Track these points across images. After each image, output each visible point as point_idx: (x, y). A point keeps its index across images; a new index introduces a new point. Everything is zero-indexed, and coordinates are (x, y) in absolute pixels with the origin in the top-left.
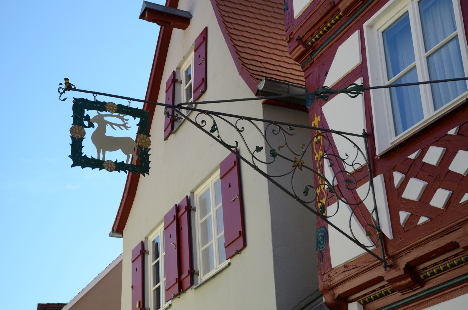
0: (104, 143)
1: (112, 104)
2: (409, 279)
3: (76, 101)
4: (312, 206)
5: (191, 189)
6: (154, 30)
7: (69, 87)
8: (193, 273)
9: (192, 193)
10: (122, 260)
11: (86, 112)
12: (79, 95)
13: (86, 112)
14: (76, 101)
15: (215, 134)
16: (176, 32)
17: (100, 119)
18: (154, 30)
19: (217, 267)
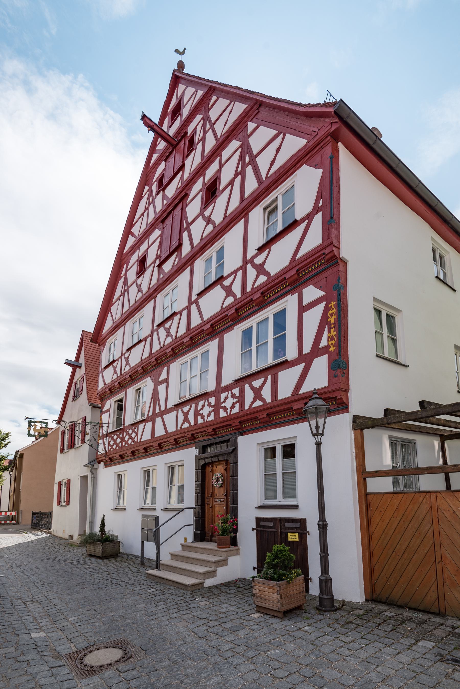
0: (35, 430)
2: (269, 377)
3: (29, 421)
6: (70, 369)
7: (27, 418)
8: (74, 444)
10: (223, 247)
11: (31, 424)
12: (29, 420)
13: (31, 424)
14: (29, 421)
16: (78, 369)
18: (70, 369)
19: (80, 445)
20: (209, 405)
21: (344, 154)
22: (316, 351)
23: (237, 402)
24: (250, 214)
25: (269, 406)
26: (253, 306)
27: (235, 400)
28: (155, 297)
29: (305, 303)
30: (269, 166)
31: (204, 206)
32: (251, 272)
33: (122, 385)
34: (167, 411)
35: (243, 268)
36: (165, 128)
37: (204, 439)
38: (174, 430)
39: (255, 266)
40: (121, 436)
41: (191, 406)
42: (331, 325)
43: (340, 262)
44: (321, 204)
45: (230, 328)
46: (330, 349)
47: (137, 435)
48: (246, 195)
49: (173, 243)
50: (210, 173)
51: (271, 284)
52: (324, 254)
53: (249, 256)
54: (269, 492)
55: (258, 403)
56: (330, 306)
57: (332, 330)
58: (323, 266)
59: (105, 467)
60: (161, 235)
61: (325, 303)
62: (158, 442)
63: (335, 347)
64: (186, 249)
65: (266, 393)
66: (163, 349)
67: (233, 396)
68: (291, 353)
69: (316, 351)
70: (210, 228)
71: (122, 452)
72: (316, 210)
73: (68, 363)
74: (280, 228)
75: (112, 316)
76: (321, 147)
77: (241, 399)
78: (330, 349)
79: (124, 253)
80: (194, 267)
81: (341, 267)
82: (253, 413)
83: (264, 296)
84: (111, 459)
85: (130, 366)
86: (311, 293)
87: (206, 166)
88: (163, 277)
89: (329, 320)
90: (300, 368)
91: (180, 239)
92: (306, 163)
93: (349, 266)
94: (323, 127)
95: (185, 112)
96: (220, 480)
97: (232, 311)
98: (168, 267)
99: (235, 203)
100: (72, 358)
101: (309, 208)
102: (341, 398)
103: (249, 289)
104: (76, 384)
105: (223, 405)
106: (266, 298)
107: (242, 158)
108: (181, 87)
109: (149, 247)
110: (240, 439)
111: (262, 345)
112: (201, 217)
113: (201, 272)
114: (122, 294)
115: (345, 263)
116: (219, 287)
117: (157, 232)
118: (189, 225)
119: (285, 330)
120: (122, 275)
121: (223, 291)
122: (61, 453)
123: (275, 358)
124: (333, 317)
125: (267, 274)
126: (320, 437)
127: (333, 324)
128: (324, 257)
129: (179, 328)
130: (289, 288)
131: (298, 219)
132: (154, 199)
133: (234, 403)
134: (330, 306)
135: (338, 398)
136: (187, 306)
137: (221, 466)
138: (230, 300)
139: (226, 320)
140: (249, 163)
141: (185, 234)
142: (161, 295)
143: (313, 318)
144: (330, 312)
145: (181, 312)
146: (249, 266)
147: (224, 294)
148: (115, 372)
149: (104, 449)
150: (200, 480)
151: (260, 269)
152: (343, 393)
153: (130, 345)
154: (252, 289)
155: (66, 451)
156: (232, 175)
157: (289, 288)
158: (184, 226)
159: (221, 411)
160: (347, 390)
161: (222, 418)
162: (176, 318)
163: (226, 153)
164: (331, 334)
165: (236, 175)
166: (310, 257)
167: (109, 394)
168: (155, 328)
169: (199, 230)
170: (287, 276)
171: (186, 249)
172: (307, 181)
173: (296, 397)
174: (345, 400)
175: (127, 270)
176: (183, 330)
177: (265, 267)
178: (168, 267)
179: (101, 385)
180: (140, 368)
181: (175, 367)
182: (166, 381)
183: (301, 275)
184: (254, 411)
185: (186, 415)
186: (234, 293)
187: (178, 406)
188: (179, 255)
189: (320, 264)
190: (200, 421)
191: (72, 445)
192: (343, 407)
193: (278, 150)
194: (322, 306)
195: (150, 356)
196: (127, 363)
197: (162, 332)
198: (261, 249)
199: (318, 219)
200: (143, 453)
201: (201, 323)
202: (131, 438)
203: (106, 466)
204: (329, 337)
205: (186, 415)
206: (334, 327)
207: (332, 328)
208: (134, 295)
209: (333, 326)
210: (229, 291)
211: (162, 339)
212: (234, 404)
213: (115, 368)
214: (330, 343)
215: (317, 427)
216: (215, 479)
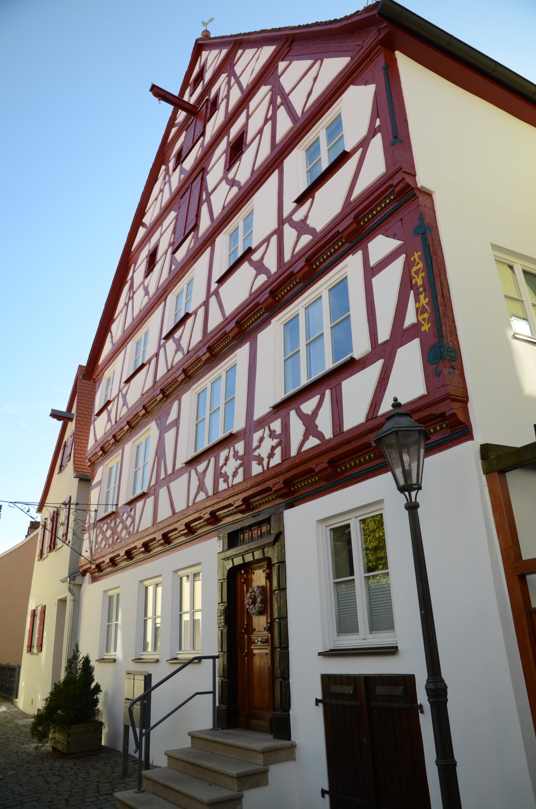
6: (59, 424)
18: (59, 424)
20: (260, 460)
21: (406, 65)
22: (401, 335)
23: (277, 446)
24: (286, 162)
25: (330, 445)
26: (297, 283)
27: (276, 441)
28: (165, 300)
29: (373, 262)
30: (305, 99)
31: (228, 167)
32: (290, 233)
33: (118, 438)
34: (176, 474)
35: (279, 232)
36: (186, 98)
37: (232, 521)
38: (185, 507)
39: (294, 225)
40: (112, 524)
41: (209, 461)
42: (418, 289)
43: (418, 194)
44: (378, 123)
45: (266, 322)
46: (423, 329)
47: (133, 522)
48: (279, 138)
49: (189, 221)
50: (234, 131)
51: (319, 245)
52: (391, 186)
53: (286, 213)
54: (345, 623)
55: (313, 442)
56: (412, 259)
57: (422, 297)
58: (396, 204)
59: (93, 582)
60: (177, 218)
61: (403, 256)
62: (162, 532)
63: (430, 324)
64: (205, 224)
65: (325, 424)
66: (171, 372)
67: (272, 434)
68: (361, 347)
69: (401, 335)
70: (235, 190)
71: (113, 552)
72: (372, 132)
73: (55, 415)
74: (325, 165)
75: (112, 337)
76: (371, 60)
77: (284, 440)
78: (423, 329)
79: (132, 250)
80: (214, 246)
81: (422, 199)
82: (305, 462)
83: (311, 265)
84: (99, 568)
85: (128, 407)
86: (381, 246)
88: (175, 269)
89: (414, 282)
90: (376, 368)
91: (198, 216)
92: (354, 83)
93: (436, 198)
94: (371, 38)
95: (208, 76)
96: (259, 600)
97: (266, 294)
98: (181, 254)
99: (265, 151)
100: (63, 408)
101: (363, 131)
102: (454, 415)
103: (287, 257)
104: (65, 446)
105: (256, 453)
106: (314, 267)
107: (272, 101)
108: (204, 54)
109: (162, 235)
110: (289, 515)
111: (314, 341)
112: (224, 182)
113: (223, 251)
114: (127, 305)
115: (429, 195)
116: (246, 265)
117: (173, 215)
118: (209, 195)
119: (348, 310)
120: (128, 279)
121: (252, 269)
123: (335, 360)
124: (420, 275)
125: (312, 231)
126: (413, 494)
127: (421, 286)
128: (393, 191)
129: (192, 336)
130: (347, 245)
131: (348, 149)
132: (170, 177)
133: (273, 447)
134: (412, 259)
135: (447, 414)
136: (205, 302)
137: (261, 570)
138: (262, 279)
139: (258, 310)
140: (282, 104)
142: (173, 294)
143: (388, 283)
144: (415, 269)
145: (195, 312)
146: (287, 227)
147: (253, 272)
149: (89, 550)
150: (225, 599)
151: (302, 227)
152: (456, 405)
154: (292, 257)
156: (261, 123)
157: (347, 245)
158: (203, 196)
159: (254, 463)
160: (464, 400)
161: (255, 476)
162: (189, 322)
163: (253, 104)
164: (421, 303)
165: (266, 121)
166: (371, 195)
167: (101, 456)
168: (214, 286)
169: (221, 198)
170: (341, 228)
171: (205, 224)
172: (358, 104)
173: (374, 421)
174: (461, 417)
175: (134, 271)
176: (197, 337)
177: (308, 222)
178: (181, 254)
181: (188, 398)
182: (176, 423)
183: (362, 223)
184: (308, 458)
185: (202, 477)
186: (266, 268)
187: (192, 462)
188: (195, 236)
189: (388, 201)
190: (222, 486)
192: (461, 431)
193: (315, 79)
194: (400, 261)
195: (153, 386)
196: (125, 403)
197: (171, 345)
198: (300, 201)
199: (377, 143)
200: (142, 552)
201: (223, 322)
202: (125, 527)
203: (94, 579)
204: (417, 309)
205: (202, 477)
206: (424, 290)
207: (421, 293)
208: (140, 300)
209: (421, 289)
210: (260, 267)
211: (173, 356)
212: (273, 448)
214: (420, 318)
215: (407, 474)
216: (251, 598)
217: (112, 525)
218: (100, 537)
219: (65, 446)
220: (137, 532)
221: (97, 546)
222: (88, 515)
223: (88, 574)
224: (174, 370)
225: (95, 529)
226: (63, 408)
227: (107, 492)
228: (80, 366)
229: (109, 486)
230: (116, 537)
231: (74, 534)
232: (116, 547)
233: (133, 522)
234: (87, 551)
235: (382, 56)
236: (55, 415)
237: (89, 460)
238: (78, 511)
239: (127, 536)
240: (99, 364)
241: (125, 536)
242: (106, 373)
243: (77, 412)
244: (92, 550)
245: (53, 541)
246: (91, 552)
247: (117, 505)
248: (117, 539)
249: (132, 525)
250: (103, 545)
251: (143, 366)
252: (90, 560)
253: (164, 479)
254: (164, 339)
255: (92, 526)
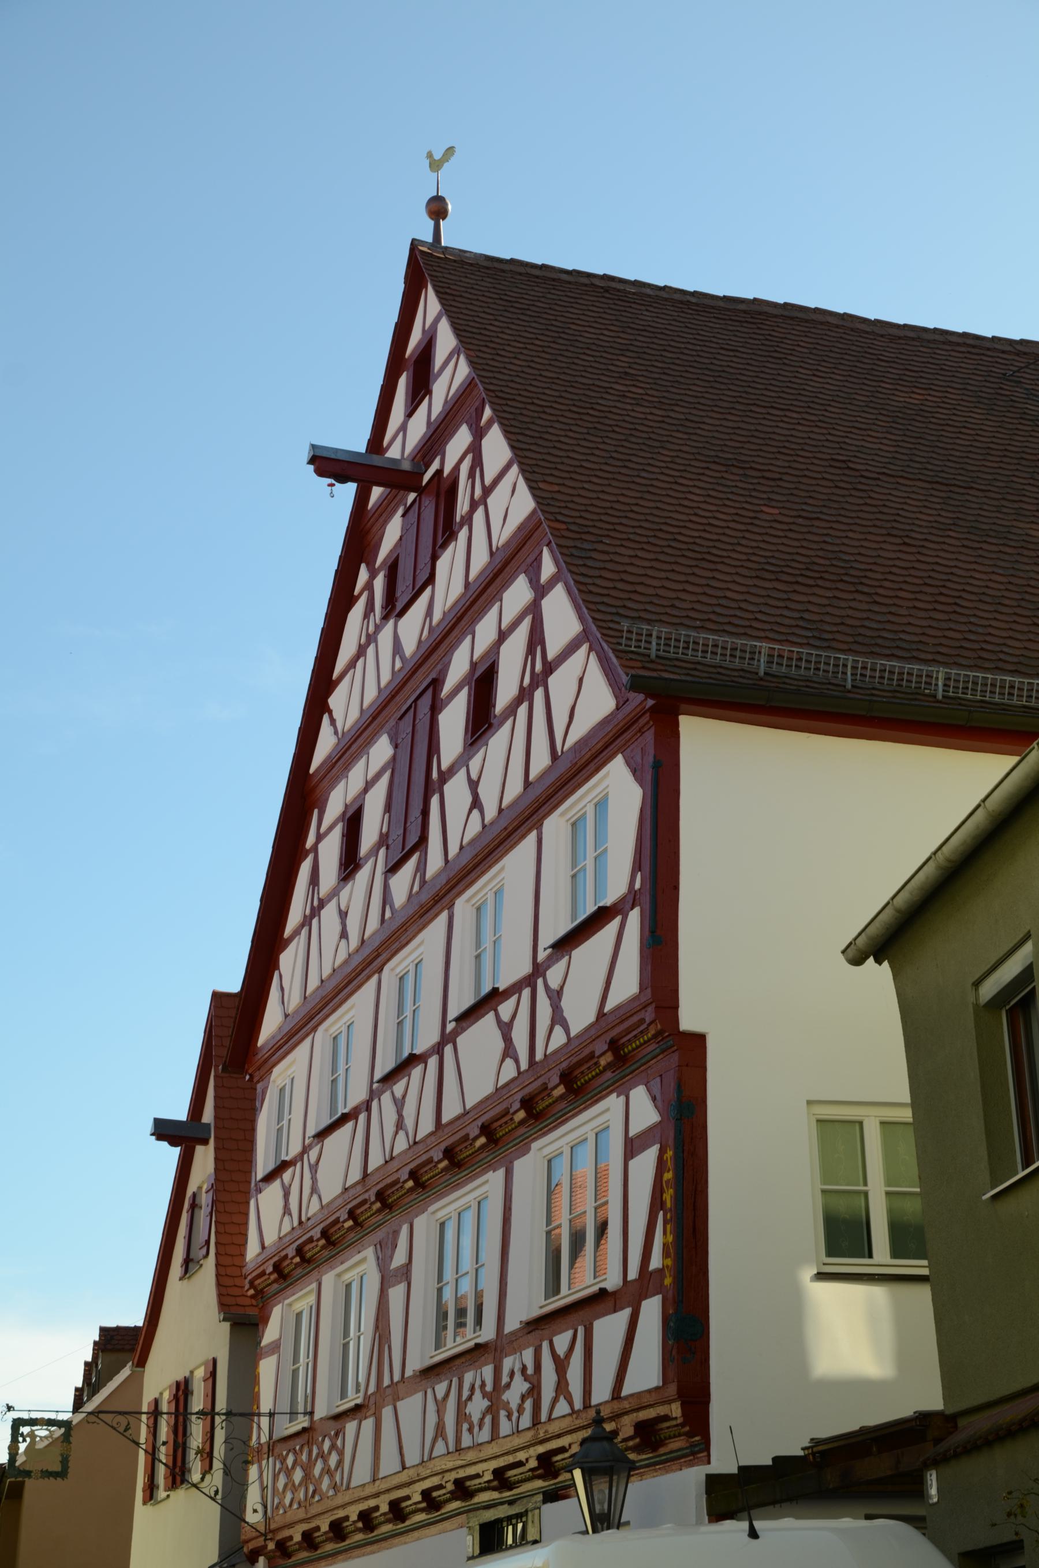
1: (42, 1419)
4: (206, 1490)
5: (191, 1368)
6: (171, 1154)
7: (9, 1408)
9: (192, 1372)
15: (127, 1434)
17: (32, 1435)
18: (171, 1154)
47: (340, 1463)
73: (164, 1130)
76: (640, 731)
85: (567, 1031)
87: (475, 608)
100: (180, 1112)
122: (145, 1503)
141: (435, 801)
148: (509, 1051)
149: (259, 1508)
153: (326, 1121)
155: (162, 1494)
168: (450, 1027)
179: (252, 1250)
180: (600, 1047)
191: (178, 1476)
213: (506, 1029)
217: (304, 1457)
218: (282, 1480)
219: (194, 1206)
220: (348, 1488)
221: (276, 1501)
222: (255, 1426)
223: (261, 1559)
224: (395, 1165)
225: (271, 1459)
226: (180, 1112)
227: (294, 1371)
228: (218, 998)
229: (296, 1359)
230: (311, 1489)
231: (227, 1472)
232: (313, 1511)
233: (340, 1463)
234: (255, 1511)
235: (649, 736)
236: (164, 1130)
237: (251, 1283)
238: (234, 1419)
239: (331, 1493)
240: (259, 1044)
241: (327, 1491)
242: (276, 1070)
243: (216, 1117)
244: (265, 1507)
245: (179, 1464)
246: (266, 1512)
247: (312, 1413)
248: (314, 1492)
249: (340, 1469)
250: (287, 1501)
251: (344, 1119)
252: (262, 1529)
253: (388, 1387)
254: (378, 1082)
255: (265, 1449)
